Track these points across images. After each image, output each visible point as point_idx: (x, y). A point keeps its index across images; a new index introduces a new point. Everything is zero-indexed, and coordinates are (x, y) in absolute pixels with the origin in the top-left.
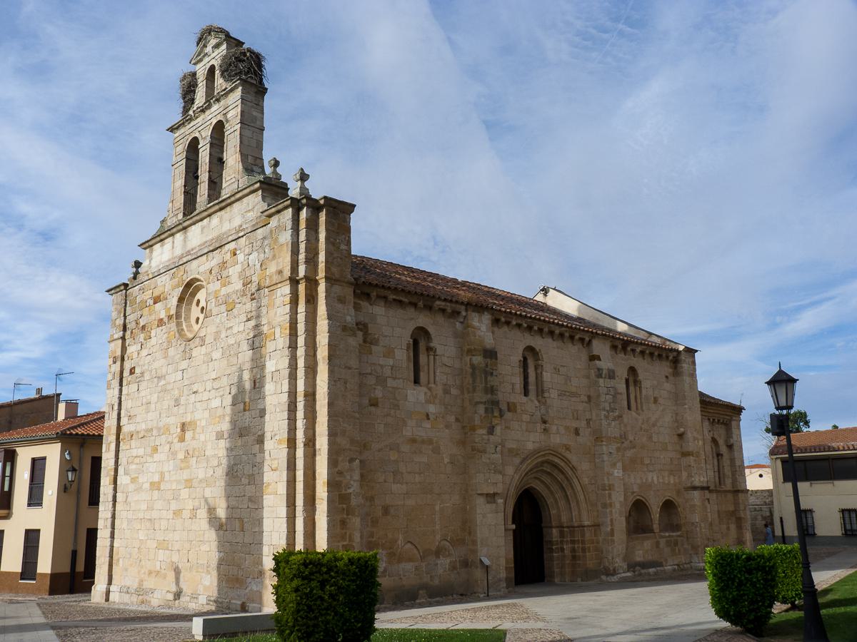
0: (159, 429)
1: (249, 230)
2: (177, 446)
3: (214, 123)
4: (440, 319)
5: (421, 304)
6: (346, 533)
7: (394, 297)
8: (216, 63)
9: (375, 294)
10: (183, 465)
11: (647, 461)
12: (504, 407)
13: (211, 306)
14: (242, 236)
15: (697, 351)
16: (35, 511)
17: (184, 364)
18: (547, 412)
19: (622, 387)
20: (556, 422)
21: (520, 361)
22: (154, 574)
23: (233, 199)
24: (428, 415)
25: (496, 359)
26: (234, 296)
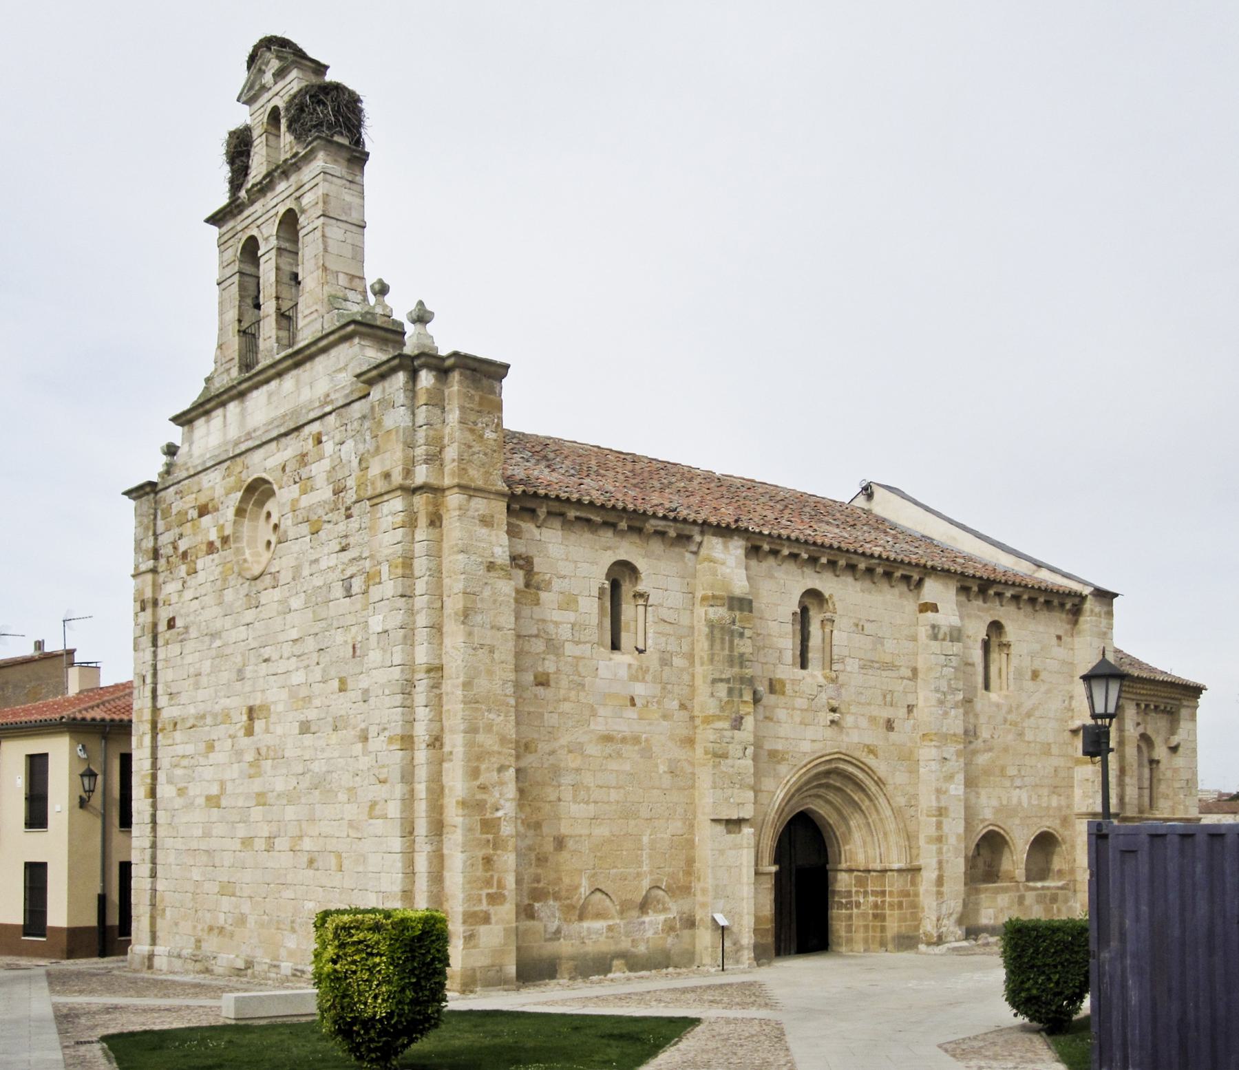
0: (215, 716)
1: (340, 403)
2: (245, 742)
3: (280, 214)
4: (656, 546)
5: (623, 525)
6: (492, 876)
7: (578, 514)
8: (280, 102)
9: (544, 509)
10: (252, 771)
11: (1012, 771)
12: (762, 688)
13: (287, 523)
14: (330, 413)
15: (1116, 595)
16: (36, 836)
17: (249, 615)
18: (839, 695)
19: (977, 655)
20: (853, 709)
21: (794, 614)
22: (216, 931)
23: (313, 349)
24: (632, 699)
25: (751, 611)
26: (321, 512)
